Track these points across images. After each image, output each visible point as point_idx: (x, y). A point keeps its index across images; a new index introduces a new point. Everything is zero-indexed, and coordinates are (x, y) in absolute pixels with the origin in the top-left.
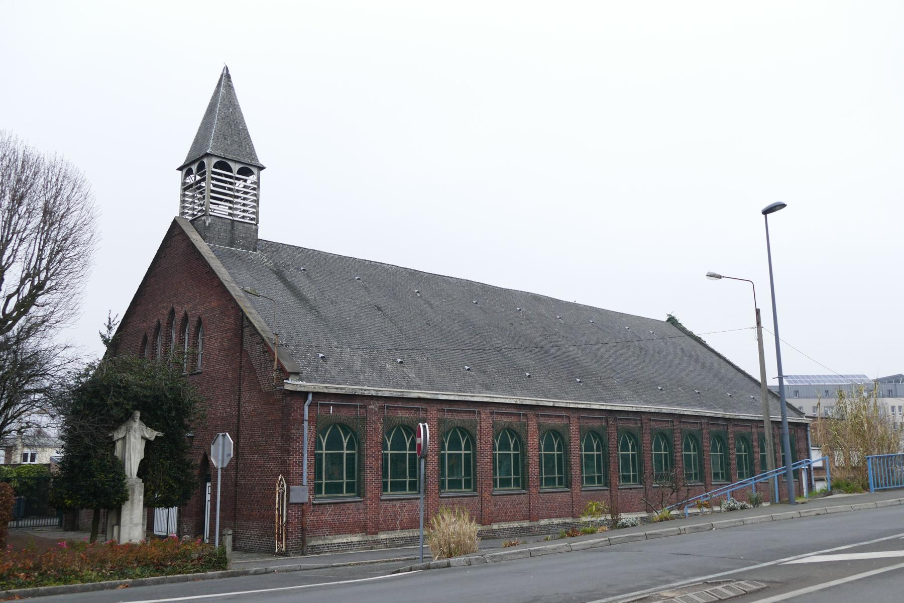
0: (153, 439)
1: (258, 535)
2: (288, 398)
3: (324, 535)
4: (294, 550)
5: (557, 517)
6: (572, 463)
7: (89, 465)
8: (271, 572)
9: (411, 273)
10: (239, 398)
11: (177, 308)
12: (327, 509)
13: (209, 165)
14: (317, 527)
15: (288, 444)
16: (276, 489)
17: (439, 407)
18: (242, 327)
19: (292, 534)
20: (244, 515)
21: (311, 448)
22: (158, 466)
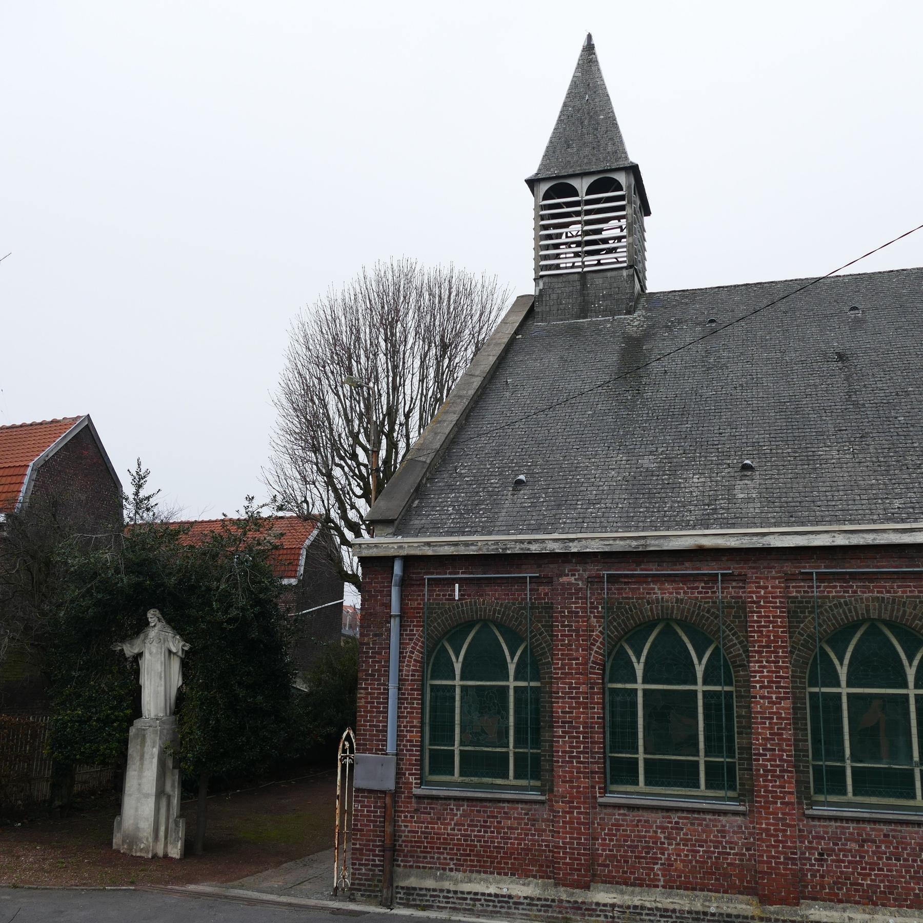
3: (444, 869)
4: (365, 891)
12: (452, 810)
14: (426, 847)
17: (788, 568)
19: (362, 854)
21: (413, 675)
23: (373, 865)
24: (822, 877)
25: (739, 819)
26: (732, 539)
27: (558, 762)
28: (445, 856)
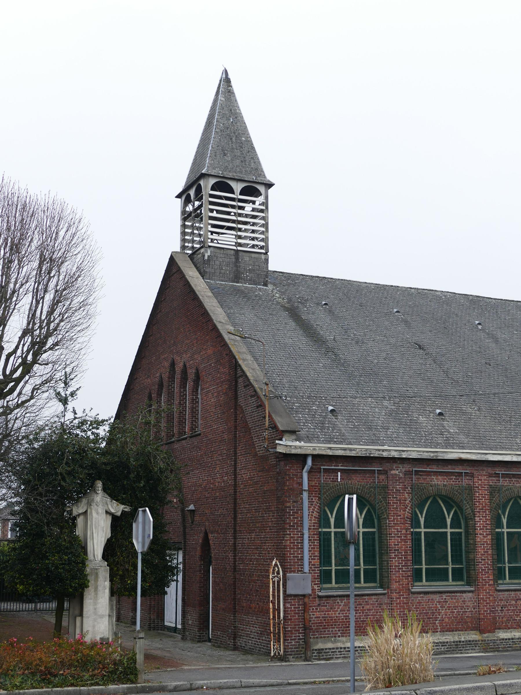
0: (119, 514)
1: (258, 633)
2: (282, 463)
3: (335, 637)
4: (294, 655)
7: (41, 545)
8: (197, 689)
9: (472, 300)
11: (177, 358)
12: (338, 603)
13: (206, 187)
14: (325, 626)
15: (283, 521)
16: (269, 576)
17: (490, 470)
18: (236, 377)
19: (292, 634)
20: (243, 607)
21: (314, 526)
22: (126, 546)
23: (298, 639)
24: (502, 618)
25: (470, 594)
26: (473, 455)
27: (393, 572)
28: (336, 629)
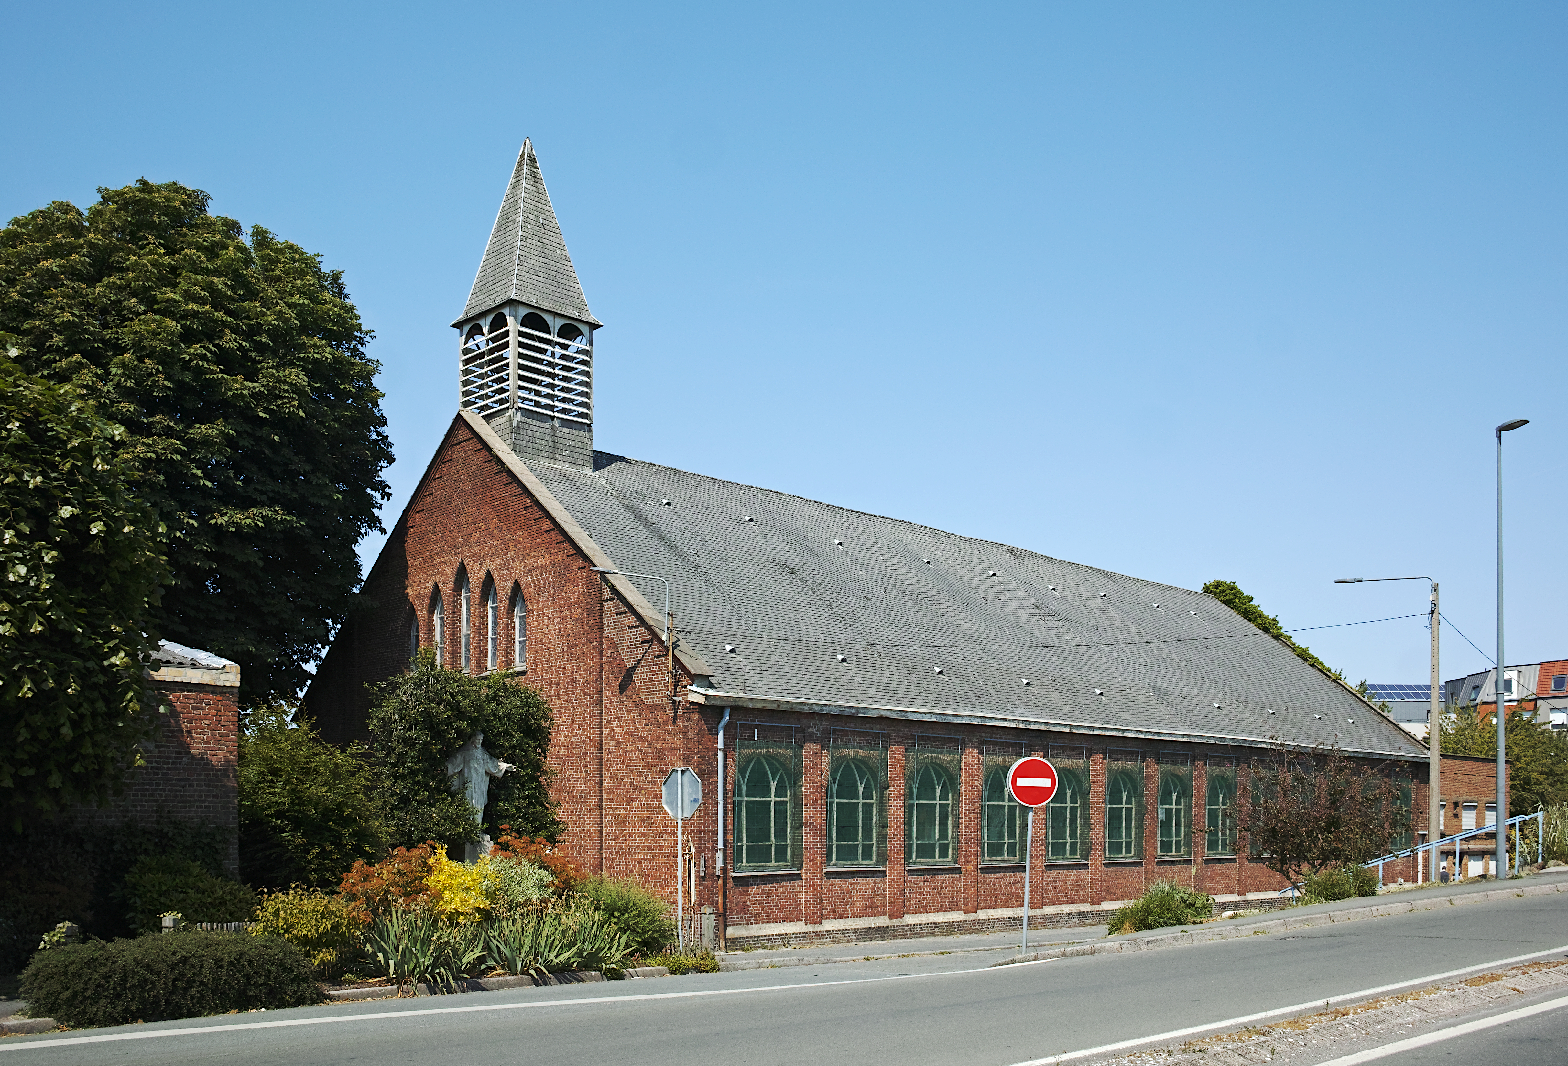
5: (1068, 903)
6: (1093, 821)
10: (601, 714)
11: (470, 564)
17: (906, 731)
